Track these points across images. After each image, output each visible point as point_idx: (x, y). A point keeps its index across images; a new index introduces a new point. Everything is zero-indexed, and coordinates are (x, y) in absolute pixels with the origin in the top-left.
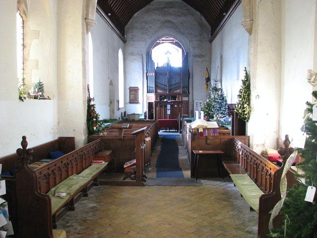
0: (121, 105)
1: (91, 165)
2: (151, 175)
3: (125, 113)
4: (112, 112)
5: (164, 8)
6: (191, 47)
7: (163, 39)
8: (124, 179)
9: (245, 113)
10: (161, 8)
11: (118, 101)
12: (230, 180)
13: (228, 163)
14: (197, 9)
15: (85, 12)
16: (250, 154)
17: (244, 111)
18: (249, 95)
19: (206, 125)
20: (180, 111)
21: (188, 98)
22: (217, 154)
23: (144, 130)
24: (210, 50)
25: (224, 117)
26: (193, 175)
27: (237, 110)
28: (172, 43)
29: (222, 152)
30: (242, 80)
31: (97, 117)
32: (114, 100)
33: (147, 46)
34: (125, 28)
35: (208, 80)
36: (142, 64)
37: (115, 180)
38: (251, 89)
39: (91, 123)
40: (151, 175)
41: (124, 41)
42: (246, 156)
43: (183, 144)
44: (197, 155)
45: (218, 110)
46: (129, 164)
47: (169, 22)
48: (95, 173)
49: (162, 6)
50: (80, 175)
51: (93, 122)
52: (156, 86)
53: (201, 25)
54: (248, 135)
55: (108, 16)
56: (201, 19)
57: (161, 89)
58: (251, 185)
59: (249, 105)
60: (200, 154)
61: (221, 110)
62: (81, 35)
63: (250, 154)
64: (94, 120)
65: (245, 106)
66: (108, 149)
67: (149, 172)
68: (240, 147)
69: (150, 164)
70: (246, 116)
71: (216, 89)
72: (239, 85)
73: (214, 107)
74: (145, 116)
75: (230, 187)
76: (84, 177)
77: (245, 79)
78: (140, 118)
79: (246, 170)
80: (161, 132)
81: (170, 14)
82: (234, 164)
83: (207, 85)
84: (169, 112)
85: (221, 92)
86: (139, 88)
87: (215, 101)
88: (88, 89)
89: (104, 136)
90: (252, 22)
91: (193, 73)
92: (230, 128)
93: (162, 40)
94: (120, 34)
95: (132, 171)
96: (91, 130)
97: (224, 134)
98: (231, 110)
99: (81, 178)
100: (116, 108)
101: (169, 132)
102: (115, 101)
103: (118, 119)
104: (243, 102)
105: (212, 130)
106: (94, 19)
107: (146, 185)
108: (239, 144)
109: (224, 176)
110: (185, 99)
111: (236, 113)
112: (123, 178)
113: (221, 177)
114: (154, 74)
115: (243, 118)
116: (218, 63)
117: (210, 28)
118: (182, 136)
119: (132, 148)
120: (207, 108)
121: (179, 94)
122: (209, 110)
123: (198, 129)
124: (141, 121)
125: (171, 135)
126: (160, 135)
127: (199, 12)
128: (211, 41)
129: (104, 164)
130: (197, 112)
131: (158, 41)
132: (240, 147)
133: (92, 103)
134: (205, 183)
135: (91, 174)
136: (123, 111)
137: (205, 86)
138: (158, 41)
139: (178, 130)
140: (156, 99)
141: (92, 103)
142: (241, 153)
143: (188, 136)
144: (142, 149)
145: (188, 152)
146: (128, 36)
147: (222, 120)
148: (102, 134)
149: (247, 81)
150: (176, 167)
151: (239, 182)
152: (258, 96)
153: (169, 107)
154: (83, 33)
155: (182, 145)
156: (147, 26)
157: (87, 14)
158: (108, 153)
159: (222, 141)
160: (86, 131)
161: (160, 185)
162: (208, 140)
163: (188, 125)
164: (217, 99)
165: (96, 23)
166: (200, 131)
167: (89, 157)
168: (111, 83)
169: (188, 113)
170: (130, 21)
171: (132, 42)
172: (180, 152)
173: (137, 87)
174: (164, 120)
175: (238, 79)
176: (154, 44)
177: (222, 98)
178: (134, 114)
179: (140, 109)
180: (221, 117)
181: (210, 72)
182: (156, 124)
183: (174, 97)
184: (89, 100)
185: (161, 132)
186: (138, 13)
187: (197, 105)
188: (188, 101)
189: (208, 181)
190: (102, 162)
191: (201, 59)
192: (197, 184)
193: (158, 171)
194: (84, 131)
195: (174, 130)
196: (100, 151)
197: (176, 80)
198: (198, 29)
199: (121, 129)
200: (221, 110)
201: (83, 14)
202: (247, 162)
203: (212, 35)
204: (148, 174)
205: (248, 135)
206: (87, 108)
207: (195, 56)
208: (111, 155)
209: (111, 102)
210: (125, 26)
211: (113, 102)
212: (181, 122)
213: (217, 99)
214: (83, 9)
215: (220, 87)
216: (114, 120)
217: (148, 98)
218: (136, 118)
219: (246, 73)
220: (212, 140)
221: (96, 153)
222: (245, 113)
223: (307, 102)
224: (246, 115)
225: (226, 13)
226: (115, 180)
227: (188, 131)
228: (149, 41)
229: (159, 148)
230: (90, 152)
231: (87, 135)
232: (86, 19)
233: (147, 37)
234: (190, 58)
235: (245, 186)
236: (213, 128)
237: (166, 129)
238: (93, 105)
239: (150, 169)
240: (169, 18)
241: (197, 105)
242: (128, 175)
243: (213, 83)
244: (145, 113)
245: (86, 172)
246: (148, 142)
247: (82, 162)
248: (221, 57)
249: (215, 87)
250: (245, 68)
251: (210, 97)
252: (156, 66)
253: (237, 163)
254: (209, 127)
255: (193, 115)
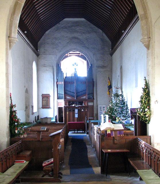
0: (35, 110)
1: (14, 164)
2: (66, 172)
3: (38, 116)
4: (27, 116)
5: (72, 26)
6: (94, 60)
7: (70, 52)
8: (43, 176)
9: (146, 116)
10: (69, 27)
11: (33, 106)
12: (137, 175)
13: (133, 160)
14: (99, 27)
15: (9, 31)
16: (154, 152)
17: (145, 115)
18: (149, 101)
19: (113, 127)
20: (86, 114)
21: (92, 103)
22: (124, 152)
23: (60, 133)
24: (111, 62)
25: (125, 119)
26: (103, 171)
27: (139, 113)
28: (78, 56)
29: (128, 151)
30: (143, 88)
31: (18, 122)
32: (29, 105)
33: (57, 59)
34: (38, 43)
35: (110, 87)
36: (52, 74)
37: (35, 177)
38: (151, 95)
39: (13, 126)
40: (66, 172)
41: (38, 55)
42: (150, 154)
43: (90, 143)
44: (106, 153)
45: (120, 113)
46: (47, 163)
47: (75, 38)
48: (18, 172)
49: (69, 25)
50: (6, 173)
51: (15, 126)
52: (65, 93)
53: (103, 40)
54: (149, 135)
55: (25, 34)
56: (103, 36)
57: (69, 95)
58: (156, 179)
59: (149, 109)
60: (109, 153)
61: (122, 113)
62: (5, 51)
63: (154, 152)
64: (16, 124)
65: (146, 110)
66: (27, 149)
67: (63, 169)
68: (143, 146)
69: (63, 162)
70: (147, 119)
71: (117, 95)
72: (140, 92)
73: (116, 111)
74: (56, 120)
75: (137, 181)
76: (9, 175)
77: (145, 87)
78: (52, 121)
79: (151, 166)
80: (70, 134)
81: (77, 32)
82: (139, 161)
83: (110, 92)
84: (76, 116)
85: (122, 97)
86: (50, 95)
87: (116, 106)
88: (11, 97)
89: (24, 138)
90: (149, 39)
91: (96, 82)
92: (133, 129)
93: (70, 54)
94: (34, 49)
95: (50, 168)
96: (13, 132)
97: (127, 134)
98: (134, 113)
99: (7, 176)
100: (30, 113)
101: (77, 133)
102: (30, 106)
103: (33, 122)
104: (144, 107)
105: (118, 132)
106: (16, 37)
107: (63, 181)
108: (143, 143)
109: (131, 171)
110: (90, 104)
111: (139, 116)
112: (42, 175)
113: (127, 172)
114: (63, 83)
115: (145, 120)
116: (118, 73)
117: (110, 42)
118: (89, 136)
119: (50, 148)
120: (110, 112)
121: (85, 100)
122: (112, 113)
123: (106, 131)
124: (53, 124)
125: (76, 136)
126: (70, 136)
127: (101, 30)
128: (112, 54)
129: (25, 163)
130: (102, 116)
131: (67, 55)
132: (143, 146)
133: (14, 109)
134: (114, 178)
135: (15, 172)
136: (36, 115)
137: (108, 93)
138: (67, 55)
139: (85, 131)
140: (65, 104)
141: (14, 109)
142: (144, 151)
143: (96, 137)
144: (59, 149)
145: (96, 150)
146: (41, 50)
147: (124, 122)
148: (22, 136)
149: (147, 88)
150: (86, 163)
151: (145, 177)
152: (157, 101)
153: (76, 111)
154: (7, 49)
155: (89, 145)
156: (57, 42)
157: (10, 33)
158: (28, 153)
159: (127, 140)
160: (9, 134)
161: (75, 181)
162: (115, 141)
163: (96, 127)
164: (119, 104)
165: (18, 41)
166: (108, 133)
167: (12, 157)
168: (27, 91)
169: (93, 116)
170: (43, 37)
171: (44, 56)
172: (88, 151)
173: (49, 94)
174: (72, 122)
175: (136, 86)
176: (63, 57)
177: (123, 103)
178: (46, 118)
179: (51, 114)
180: (123, 120)
181: (112, 80)
182: (66, 127)
183: (81, 103)
184: (12, 107)
185: (70, 134)
186: (49, 31)
187: (101, 109)
188: (93, 106)
189: (117, 176)
190: (24, 161)
191: (104, 70)
192: (108, 180)
193: (71, 168)
194: (7, 134)
195: (82, 132)
196: (22, 151)
197: (82, 88)
198: (100, 44)
199: (39, 132)
200: (122, 113)
201: (7, 33)
202: (151, 159)
203: (112, 49)
204: (63, 171)
205: (149, 135)
206: (9, 113)
207: (98, 67)
208: (30, 155)
209: (26, 108)
210: (38, 42)
211: (28, 107)
212: (88, 124)
213: (119, 104)
214: (7, 29)
215: (120, 93)
216: (29, 123)
217: (58, 103)
218: (49, 122)
219: (146, 82)
220: (119, 140)
221: (18, 154)
222: (146, 116)
223: (136, 87)
224: (147, 117)
225: (125, 31)
226: (35, 177)
227: (95, 132)
228: (59, 55)
229: (70, 147)
230: (13, 152)
231: (9, 138)
232: (9, 37)
233: (57, 51)
234: (94, 69)
235: (152, 180)
236: (119, 130)
237: (74, 131)
238: (15, 111)
239: (64, 166)
240: (76, 35)
241: (101, 109)
242: (47, 174)
243: (114, 89)
244: (56, 117)
245: (10, 171)
246: (62, 143)
247: (6, 161)
248: (121, 68)
249: (116, 94)
250: (145, 77)
251: (112, 103)
252: (65, 76)
253: (141, 160)
254: (115, 129)
255: (97, 117)
